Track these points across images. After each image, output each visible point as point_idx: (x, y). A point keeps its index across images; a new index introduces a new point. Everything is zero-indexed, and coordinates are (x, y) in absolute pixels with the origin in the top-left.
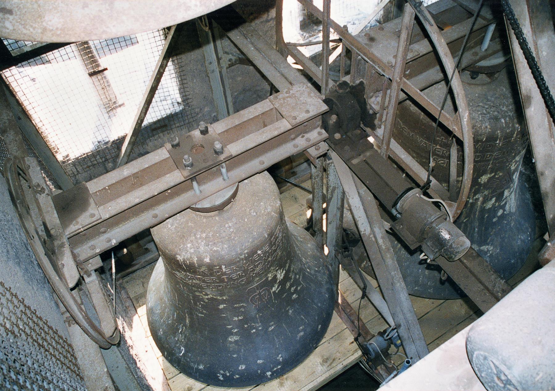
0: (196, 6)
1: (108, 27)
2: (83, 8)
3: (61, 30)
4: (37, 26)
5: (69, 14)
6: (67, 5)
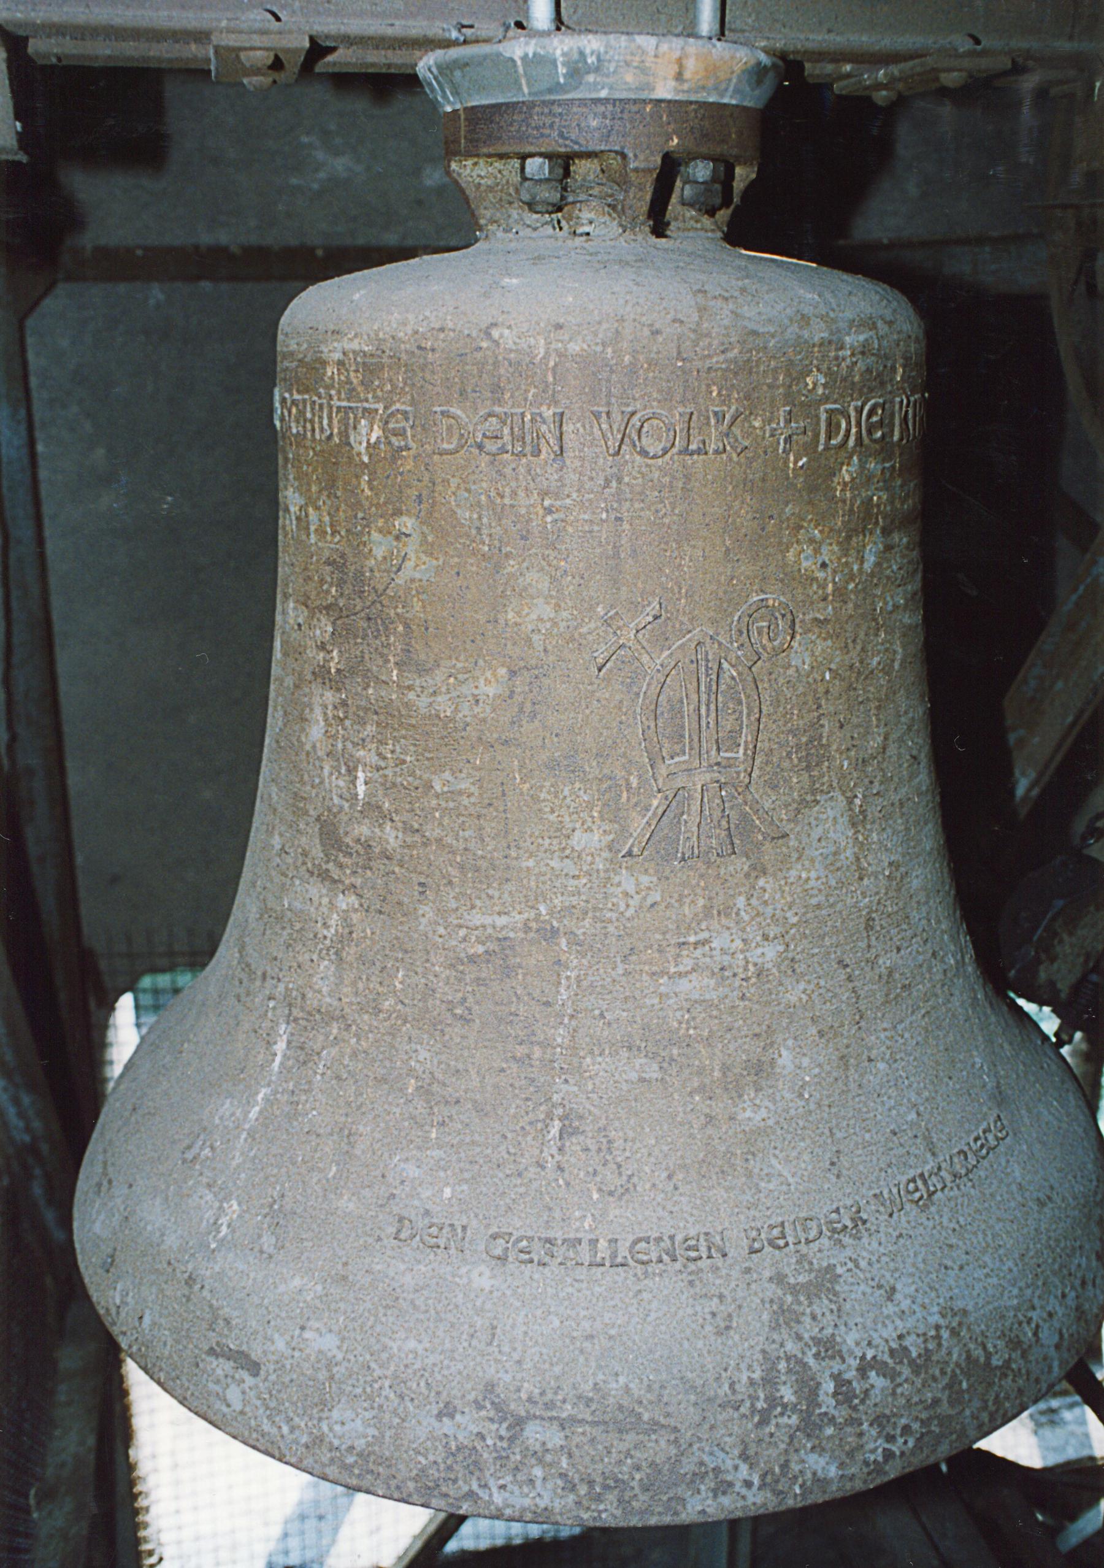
0: (748, 1484)
1: (486, 1486)
2: (439, 1416)
3: (360, 1455)
4: (303, 1424)
5: (397, 1420)
6: (401, 1397)
